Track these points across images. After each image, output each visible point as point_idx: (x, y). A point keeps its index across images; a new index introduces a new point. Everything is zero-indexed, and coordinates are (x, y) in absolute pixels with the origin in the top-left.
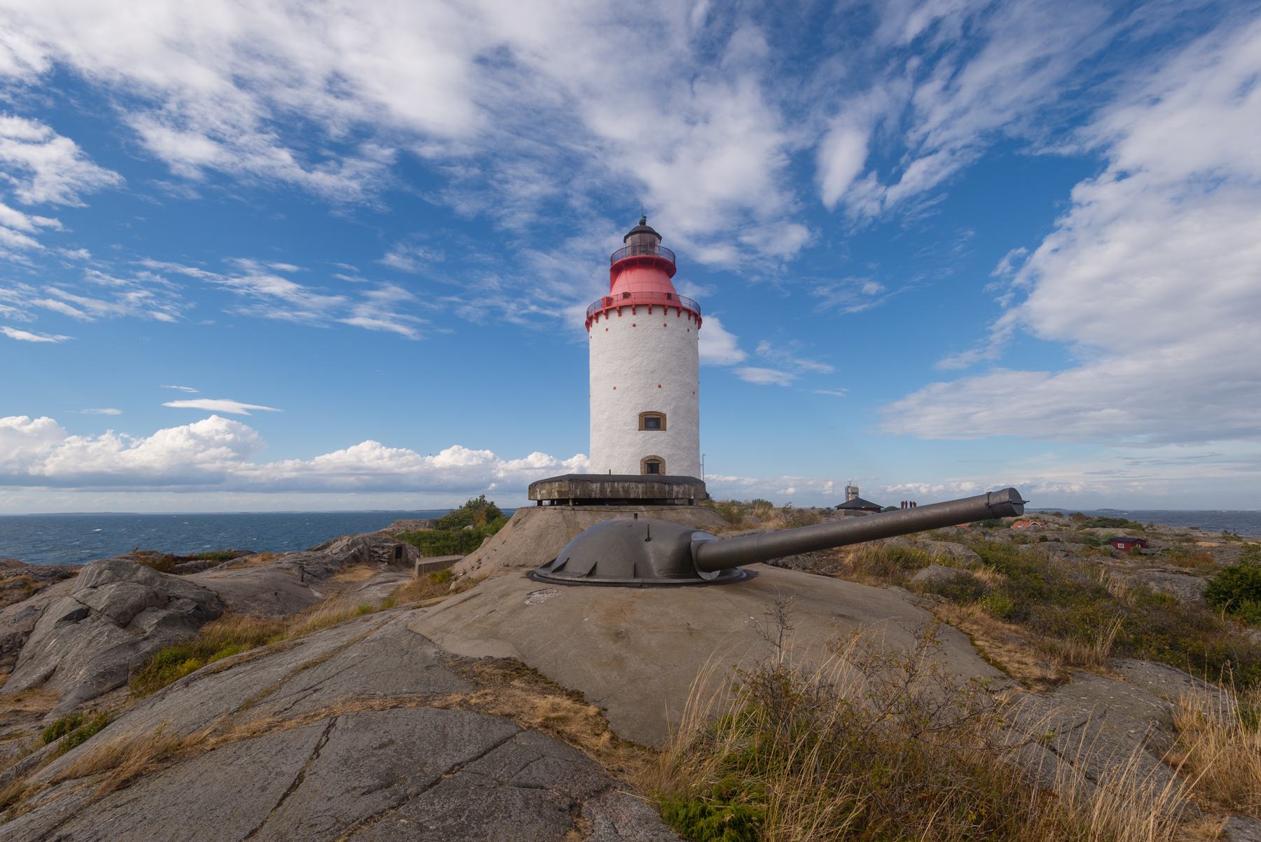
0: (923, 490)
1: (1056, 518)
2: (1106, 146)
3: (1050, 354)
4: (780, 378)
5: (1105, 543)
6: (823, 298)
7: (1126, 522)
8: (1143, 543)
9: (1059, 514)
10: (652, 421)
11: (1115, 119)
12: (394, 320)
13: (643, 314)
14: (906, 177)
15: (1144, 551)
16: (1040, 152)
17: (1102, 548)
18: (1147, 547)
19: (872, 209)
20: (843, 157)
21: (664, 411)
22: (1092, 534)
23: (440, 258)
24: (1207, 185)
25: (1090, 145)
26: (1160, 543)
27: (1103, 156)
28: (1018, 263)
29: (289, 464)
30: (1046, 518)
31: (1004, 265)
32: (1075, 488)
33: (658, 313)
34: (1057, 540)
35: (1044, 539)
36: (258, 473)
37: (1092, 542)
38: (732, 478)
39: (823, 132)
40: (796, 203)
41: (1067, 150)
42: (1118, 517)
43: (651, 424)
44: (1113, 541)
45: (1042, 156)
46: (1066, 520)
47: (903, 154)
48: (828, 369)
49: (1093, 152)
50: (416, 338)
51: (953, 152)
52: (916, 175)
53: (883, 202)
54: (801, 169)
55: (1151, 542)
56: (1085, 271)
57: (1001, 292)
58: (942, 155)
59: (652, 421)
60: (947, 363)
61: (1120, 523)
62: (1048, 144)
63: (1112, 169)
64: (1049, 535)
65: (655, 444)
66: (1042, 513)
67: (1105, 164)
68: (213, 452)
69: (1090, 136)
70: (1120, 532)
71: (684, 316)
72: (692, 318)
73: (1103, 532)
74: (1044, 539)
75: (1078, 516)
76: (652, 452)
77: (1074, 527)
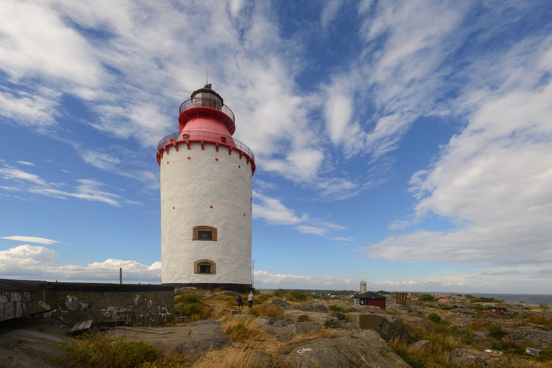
0: (392, 284)
1: (459, 297)
2: (468, 113)
3: (437, 222)
4: (319, 231)
5: (486, 309)
6: (324, 190)
7: (493, 299)
8: (505, 310)
9: (460, 295)
10: (204, 234)
11: (473, 97)
12: (103, 195)
13: (196, 149)
14: (378, 128)
15: (505, 313)
16: (429, 114)
17: (484, 311)
18: (506, 311)
19: (360, 145)
20: (339, 111)
21: (215, 226)
22: (479, 305)
23: (118, 161)
24: (517, 138)
25: (458, 112)
26: (513, 310)
27: (464, 119)
28: (424, 177)
29: (71, 267)
30: (454, 297)
31: (414, 179)
32: (460, 284)
33: (210, 150)
34: (462, 307)
35: (455, 307)
36: (56, 271)
37: (480, 309)
38: (301, 277)
39: (326, 97)
40: (314, 139)
41: (444, 113)
42: (490, 297)
43: (204, 235)
44: (490, 308)
45: (430, 117)
46: (463, 298)
47: (373, 113)
48: (341, 228)
49: (460, 117)
50: (119, 206)
51: (402, 114)
52: (385, 126)
53: (365, 141)
54: (317, 117)
55: (508, 309)
56: (456, 181)
57: (417, 191)
58: (396, 116)
59: (204, 234)
60: (394, 226)
61: (491, 300)
62: (433, 109)
63: (471, 127)
64: (458, 305)
65: (207, 250)
66: (452, 295)
67: (466, 125)
68: (27, 260)
69: (460, 105)
70: (493, 305)
71: (244, 159)
72: (250, 163)
73: (485, 304)
74: (455, 307)
75: (469, 296)
76: (204, 256)
77: (468, 301)
